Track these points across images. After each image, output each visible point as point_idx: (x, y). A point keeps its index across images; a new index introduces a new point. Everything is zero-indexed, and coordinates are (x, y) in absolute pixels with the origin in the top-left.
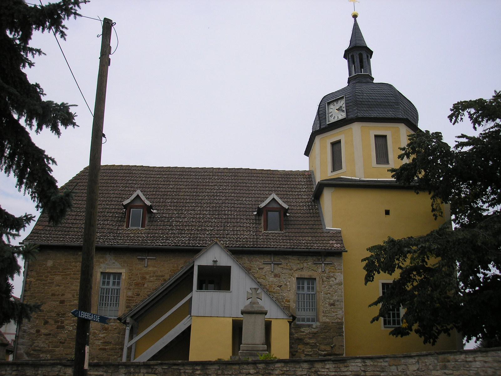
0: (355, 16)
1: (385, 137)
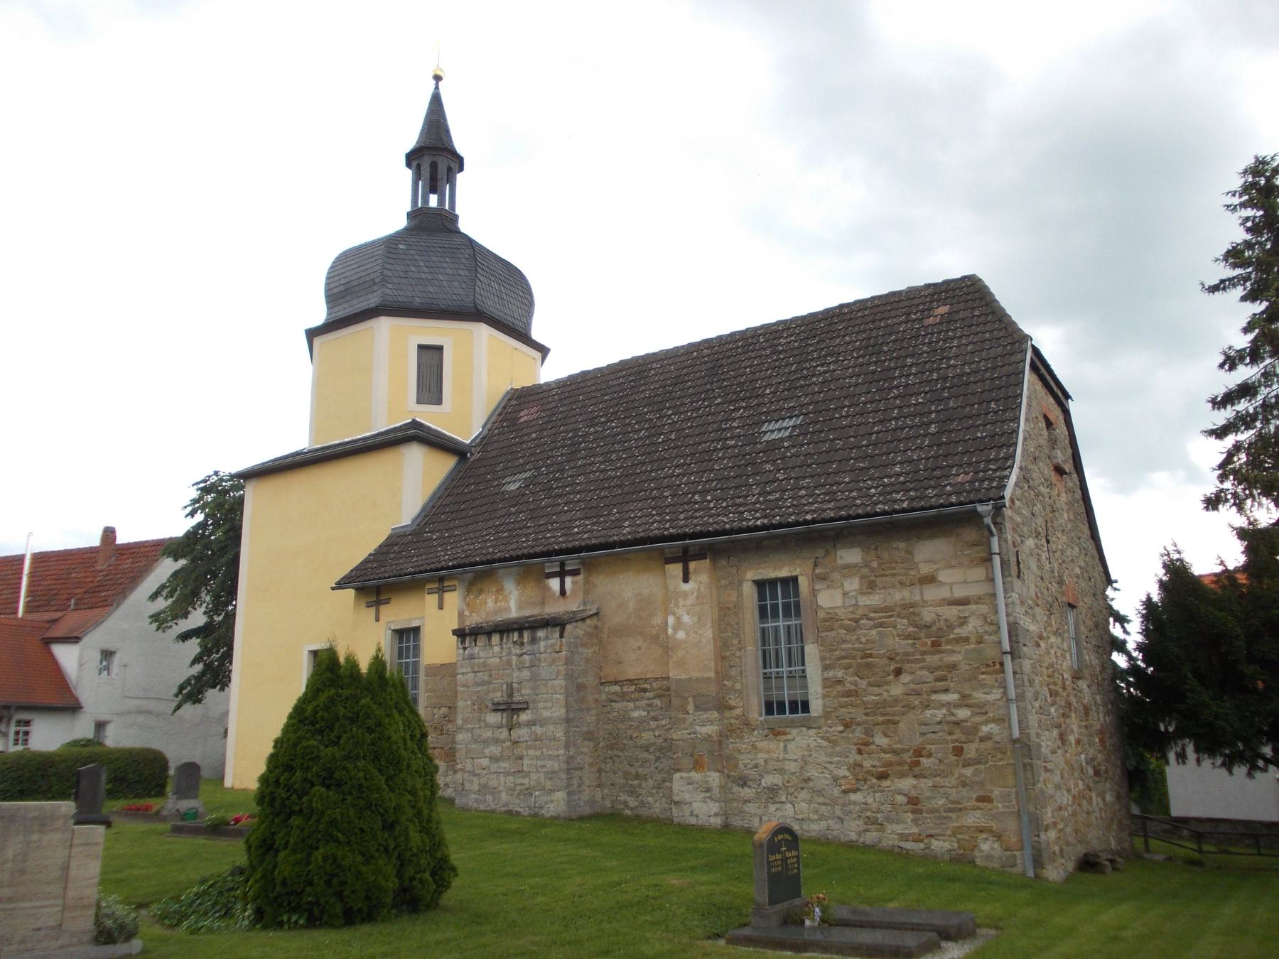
0: (438, 78)
1: (439, 349)
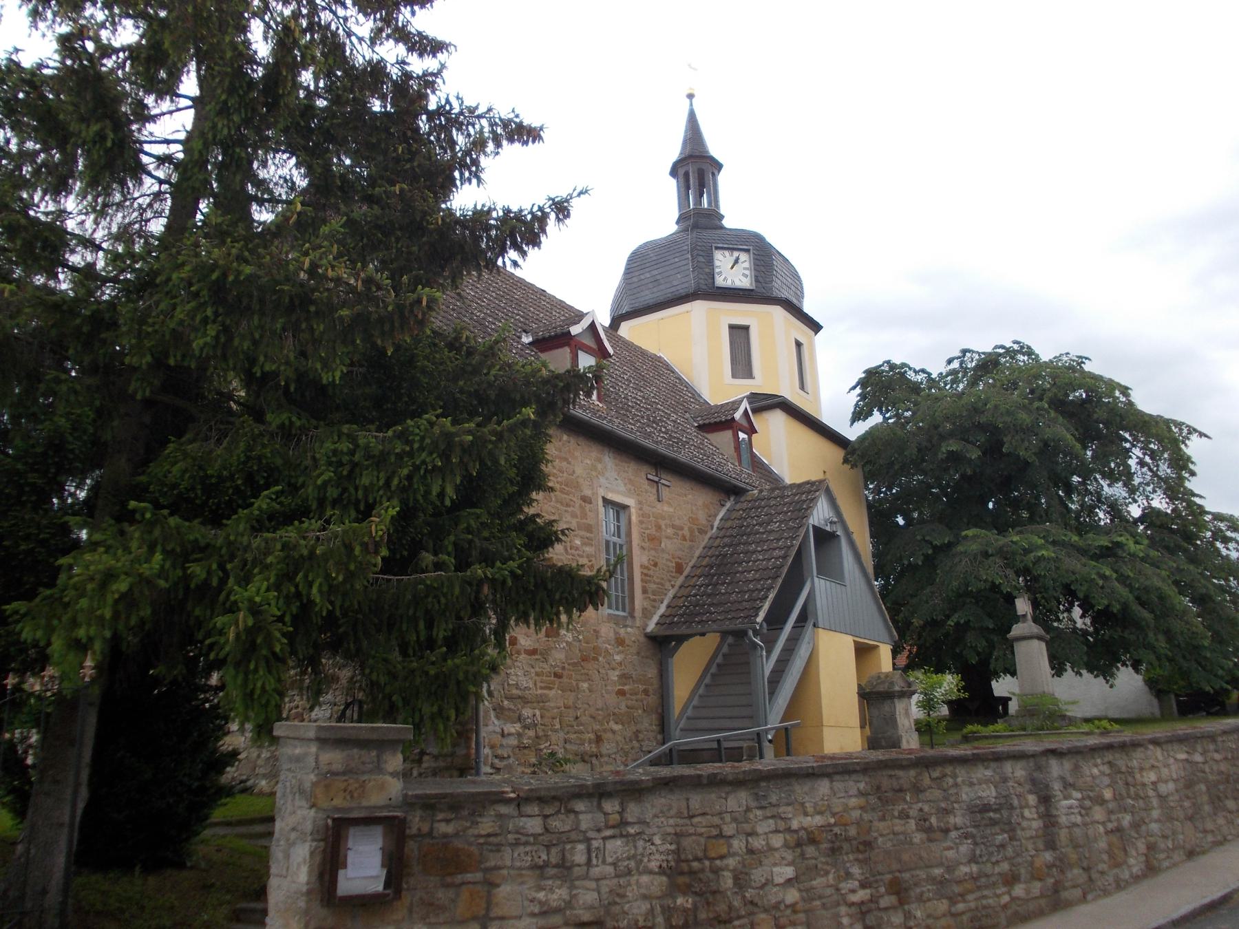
0: (691, 96)
